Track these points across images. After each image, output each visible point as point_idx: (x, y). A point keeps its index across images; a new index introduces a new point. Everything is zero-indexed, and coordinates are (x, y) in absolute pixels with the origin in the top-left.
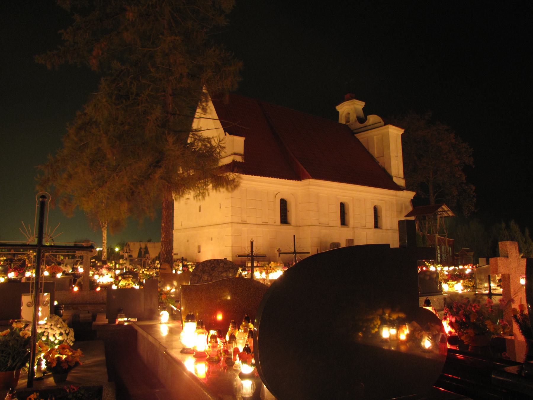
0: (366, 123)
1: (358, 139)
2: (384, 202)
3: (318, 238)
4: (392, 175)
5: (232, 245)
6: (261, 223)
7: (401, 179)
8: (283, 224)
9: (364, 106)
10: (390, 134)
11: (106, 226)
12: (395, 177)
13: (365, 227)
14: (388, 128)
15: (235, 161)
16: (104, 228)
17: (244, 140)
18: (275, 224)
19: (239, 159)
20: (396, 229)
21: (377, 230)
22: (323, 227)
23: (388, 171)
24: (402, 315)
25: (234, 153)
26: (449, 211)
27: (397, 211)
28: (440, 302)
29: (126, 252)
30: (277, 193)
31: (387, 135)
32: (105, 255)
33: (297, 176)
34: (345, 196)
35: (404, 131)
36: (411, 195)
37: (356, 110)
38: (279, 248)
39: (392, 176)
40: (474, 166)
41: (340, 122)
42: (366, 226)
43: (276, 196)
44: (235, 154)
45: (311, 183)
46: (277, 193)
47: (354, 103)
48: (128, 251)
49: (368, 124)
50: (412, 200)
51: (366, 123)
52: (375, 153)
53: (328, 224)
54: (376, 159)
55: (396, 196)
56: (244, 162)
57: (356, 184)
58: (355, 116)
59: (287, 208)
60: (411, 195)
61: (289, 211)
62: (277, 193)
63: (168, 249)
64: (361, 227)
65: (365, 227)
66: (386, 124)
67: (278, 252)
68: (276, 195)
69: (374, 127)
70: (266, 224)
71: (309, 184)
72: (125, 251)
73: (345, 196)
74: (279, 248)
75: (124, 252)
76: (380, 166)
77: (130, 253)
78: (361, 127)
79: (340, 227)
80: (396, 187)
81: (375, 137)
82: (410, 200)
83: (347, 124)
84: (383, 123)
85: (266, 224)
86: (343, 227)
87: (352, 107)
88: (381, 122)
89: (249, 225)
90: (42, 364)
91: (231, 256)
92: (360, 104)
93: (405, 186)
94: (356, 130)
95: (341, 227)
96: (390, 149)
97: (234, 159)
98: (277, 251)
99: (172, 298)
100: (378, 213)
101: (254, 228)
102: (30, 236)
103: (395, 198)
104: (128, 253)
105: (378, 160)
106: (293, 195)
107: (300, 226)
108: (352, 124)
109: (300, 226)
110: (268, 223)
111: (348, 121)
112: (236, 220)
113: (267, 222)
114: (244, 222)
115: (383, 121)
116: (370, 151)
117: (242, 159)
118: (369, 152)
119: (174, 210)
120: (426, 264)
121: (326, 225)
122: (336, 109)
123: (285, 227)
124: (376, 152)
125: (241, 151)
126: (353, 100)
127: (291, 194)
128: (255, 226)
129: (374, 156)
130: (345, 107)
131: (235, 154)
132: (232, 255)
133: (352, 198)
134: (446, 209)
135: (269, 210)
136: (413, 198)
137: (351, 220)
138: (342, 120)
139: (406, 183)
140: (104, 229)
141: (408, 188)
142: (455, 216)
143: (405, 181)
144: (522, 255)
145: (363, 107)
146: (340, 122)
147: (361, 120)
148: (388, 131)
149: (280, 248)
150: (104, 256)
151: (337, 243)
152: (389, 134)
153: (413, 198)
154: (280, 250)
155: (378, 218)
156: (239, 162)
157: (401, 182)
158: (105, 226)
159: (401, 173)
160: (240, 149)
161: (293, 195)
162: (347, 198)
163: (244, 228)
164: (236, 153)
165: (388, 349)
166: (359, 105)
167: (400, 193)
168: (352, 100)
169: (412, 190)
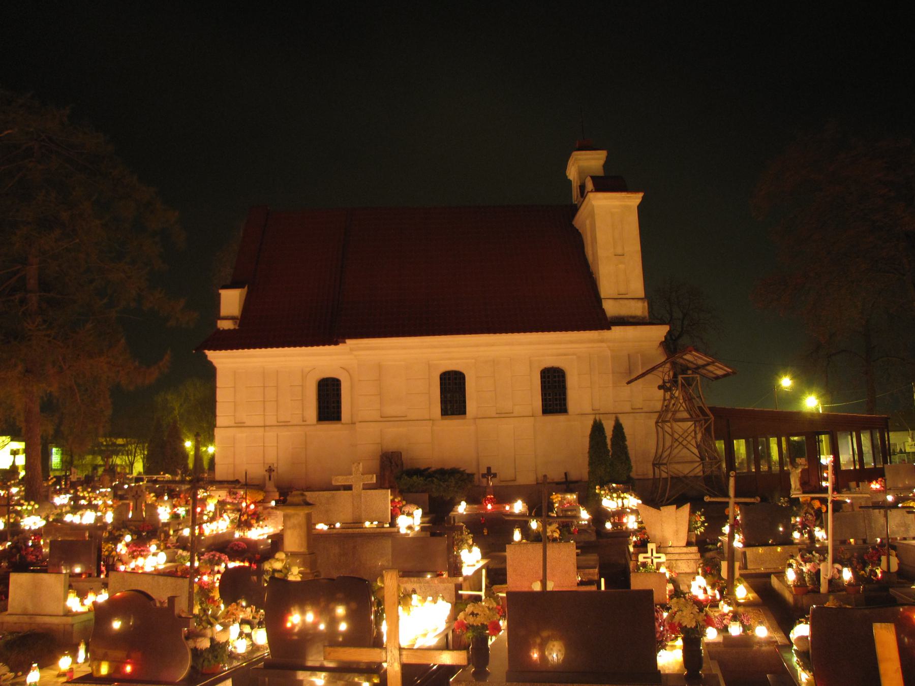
2: (575, 357)
3: (378, 444)
6: (275, 423)
7: (631, 301)
13: (511, 415)
18: (304, 423)
22: (391, 423)
24: (794, 593)
27: (613, 373)
34: (450, 359)
36: (659, 332)
42: (512, 413)
47: (580, 160)
50: (662, 343)
55: (602, 341)
60: (659, 332)
64: (497, 416)
65: (511, 415)
67: (267, 472)
70: (285, 425)
73: (450, 359)
74: (270, 467)
79: (440, 419)
85: (285, 425)
86: (446, 419)
89: (246, 429)
90: (71, 608)
93: (646, 314)
95: (442, 419)
98: (266, 471)
99: (789, 498)
100: (566, 383)
102: (697, 382)
103: (604, 345)
110: (289, 422)
113: (288, 420)
117: (234, 325)
119: (218, 404)
120: (596, 489)
127: (341, 367)
133: (509, 359)
141: (651, 320)
152: (594, 212)
156: (229, 330)
159: (637, 286)
162: (459, 361)
169: (661, 322)
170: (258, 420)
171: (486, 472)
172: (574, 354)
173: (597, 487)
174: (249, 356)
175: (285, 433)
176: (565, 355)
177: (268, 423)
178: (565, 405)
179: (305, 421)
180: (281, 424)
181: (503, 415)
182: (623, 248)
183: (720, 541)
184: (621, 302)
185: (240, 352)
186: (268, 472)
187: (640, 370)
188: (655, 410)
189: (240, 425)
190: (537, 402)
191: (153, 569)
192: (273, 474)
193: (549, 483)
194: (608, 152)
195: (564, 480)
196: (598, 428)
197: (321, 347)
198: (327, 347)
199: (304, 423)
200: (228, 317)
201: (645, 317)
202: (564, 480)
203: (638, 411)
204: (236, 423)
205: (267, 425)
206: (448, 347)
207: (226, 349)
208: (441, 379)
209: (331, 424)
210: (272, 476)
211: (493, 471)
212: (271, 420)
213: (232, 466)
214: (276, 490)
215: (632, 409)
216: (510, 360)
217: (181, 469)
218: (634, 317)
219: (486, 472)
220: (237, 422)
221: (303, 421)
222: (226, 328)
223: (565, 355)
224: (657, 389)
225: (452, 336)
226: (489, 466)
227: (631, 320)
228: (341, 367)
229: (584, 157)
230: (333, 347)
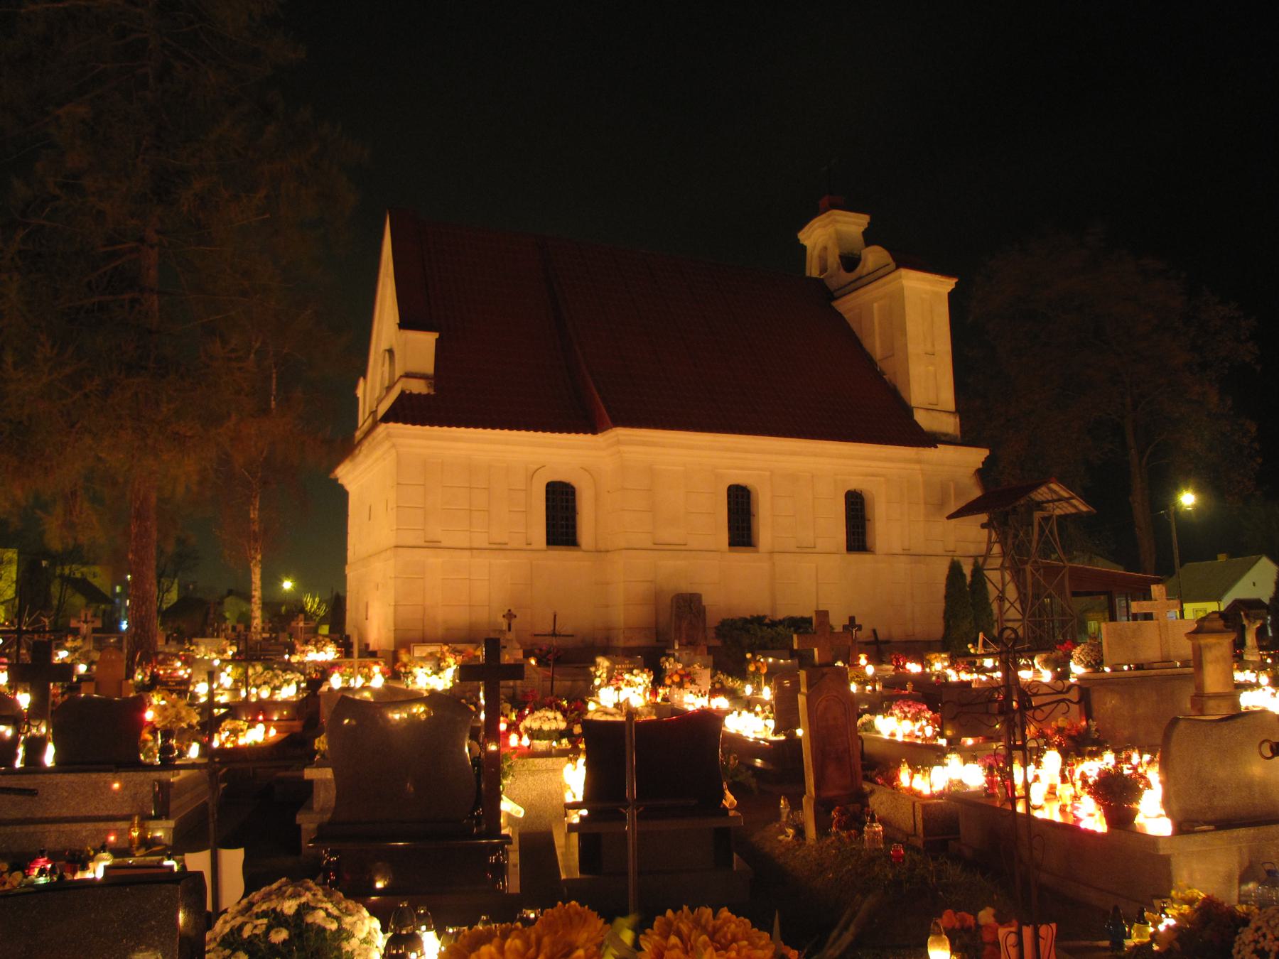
0: (861, 270)
1: (840, 314)
2: (882, 479)
3: (651, 581)
4: (913, 404)
5: (395, 602)
6: (486, 545)
7: (942, 413)
8: (550, 547)
9: (867, 226)
10: (906, 293)
11: (259, 557)
12: (920, 411)
14: (900, 277)
15: (408, 392)
16: (254, 561)
17: (437, 340)
18: (529, 547)
19: (418, 387)
20: (923, 553)
21: (856, 557)
23: (903, 394)
25: (406, 373)
26: (1073, 498)
27: (926, 503)
28: (136, 794)
29: (86, 622)
30: (538, 469)
31: (898, 299)
32: (257, 624)
33: (587, 423)
34: (742, 469)
35: (956, 283)
36: (976, 456)
37: (840, 238)
38: (510, 610)
39: (913, 407)
40: (1258, 368)
41: (808, 274)
42: (815, 547)
43: (535, 474)
44: (408, 375)
45: (621, 438)
46: (536, 467)
47: (838, 222)
48: (89, 619)
49: (865, 272)
50: (978, 471)
51: (859, 268)
52: (876, 347)
53: (685, 545)
54: (878, 364)
55: (919, 462)
56: (432, 393)
57: (771, 435)
58: (837, 252)
59: (752, 509)
60: (976, 456)
61: (754, 516)
62: (538, 469)
63: (138, 614)
64: (797, 550)
66: (898, 267)
68: (534, 474)
69: (877, 275)
70: (500, 548)
71: (619, 443)
72: (83, 619)
73: (742, 469)
74: (510, 610)
75: (79, 622)
76: (887, 381)
77: (93, 622)
78: (850, 280)
80: (930, 440)
81: (875, 305)
82: (972, 470)
83: (822, 277)
84: (893, 265)
85: (500, 548)
86: (736, 551)
87: (831, 230)
88: (888, 265)
89: (446, 552)
91: (393, 628)
92: (853, 220)
93: (958, 433)
94: (838, 290)
95: (730, 551)
96: (906, 335)
97: (405, 388)
98: (504, 616)
101: (464, 557)
103: (917, 467)
104: (90, 624)
105: (882, 365)
106: (585, 470)
107: (608, 551)
108: (831, 277)
109: (608, 551)
110: (506, 544)
111: (823, 269)
112: (410, 539)
114: (433, 545)
115: (894, 260)
116: (866, 344)
117: (429, 387)
118: (864, 345)
120: (969, 649)
121: (809, 550)
122: (799, 240)
123: (561, 555)
124: (878, 344)
125: (429, 368)
126: (830, 212)
127: (582, 468)
128: (467, 553)
129: (874, 357)
130: (816, 232)
131: (408, 375)
132: (395, 625)
133: (768, 473)
134: (1065, 494)
135: (510, 511)
136: (981, 466)
137: (765, 530)
138: (813, 270)
139: (962, 425)
140: (255, 565)
141: (966, 438)
142: (1095, 512)
143: (958, 420)
144: (1258, 625)
145: (866, 229)
146: (808, 274)
147: (850, 261)
148: (902, 288)
149: (512, 610)
150: (255, 628)
151: (691, 594)
153: (981, 466)
154: (507, 614)
155: (867, 522)
156: (419, 395)
157: (949, 424)
158: (255, 558)
159: (947, 397)
160: (427, 363)
161: (585, 470)
163: (434, 560)
164: (412, 373)
165: (365, 909)
166: (852, 224)
167: (944, 453)
168: (827, 213)
170: (461, 539)
171: (848, 623)
172: (883, 476)
173: (970, 646)
174: (455, 439)
175: (500, 561)
176: (873, 475)
177: (475, 545)
178: (574, 534)
179: (530, 544)
180: (494, 546)
181: (805, 550)
182: (933, 345)
183: (623, 716)
184: (934, 413)
185: (436, 430)
186: (507, 619)
187: (953, 502)
188: (968, 554)
189: (431, 544)
190: (539, 531)
191: (946, 761)
192: (514, 622)
193: (859, 643)
194: (871, 219)
195: (873, 639)
196: (955, 569)
197: (565, 435)
198: (573, 436)
199: (529, 547)
200: (416, 373)
201: (957, 437)
202: (873, 639)
203: (809, 550)
204: (425, 542)
205: (468, 551)
206: (746, 451)
207: (441, 425)
208: (547, 492)
209: (570, 550)
210: (512, 626)
211: (857, 622)
212: (480, 540)
213: (487, 607)
214: (518, 646)
215: (946, 551)
216: (812, 477)
217: (49, 618)
218: (946, 435)
219: (848, 623)
220: (427, 539)
221: (528, 544)
222: (416, 391)
223: (873, 475)
224: (979, 528)
225: (756, 437)
226: (853, 615)
227: (943, 438)
228: (582, 468)
229: (846, 219)
230: (589, 437)
